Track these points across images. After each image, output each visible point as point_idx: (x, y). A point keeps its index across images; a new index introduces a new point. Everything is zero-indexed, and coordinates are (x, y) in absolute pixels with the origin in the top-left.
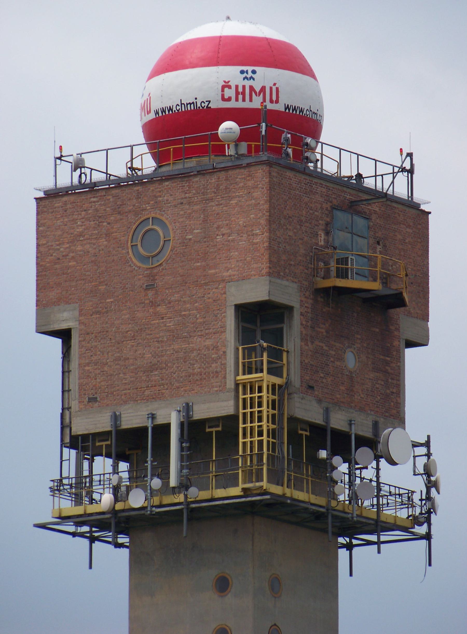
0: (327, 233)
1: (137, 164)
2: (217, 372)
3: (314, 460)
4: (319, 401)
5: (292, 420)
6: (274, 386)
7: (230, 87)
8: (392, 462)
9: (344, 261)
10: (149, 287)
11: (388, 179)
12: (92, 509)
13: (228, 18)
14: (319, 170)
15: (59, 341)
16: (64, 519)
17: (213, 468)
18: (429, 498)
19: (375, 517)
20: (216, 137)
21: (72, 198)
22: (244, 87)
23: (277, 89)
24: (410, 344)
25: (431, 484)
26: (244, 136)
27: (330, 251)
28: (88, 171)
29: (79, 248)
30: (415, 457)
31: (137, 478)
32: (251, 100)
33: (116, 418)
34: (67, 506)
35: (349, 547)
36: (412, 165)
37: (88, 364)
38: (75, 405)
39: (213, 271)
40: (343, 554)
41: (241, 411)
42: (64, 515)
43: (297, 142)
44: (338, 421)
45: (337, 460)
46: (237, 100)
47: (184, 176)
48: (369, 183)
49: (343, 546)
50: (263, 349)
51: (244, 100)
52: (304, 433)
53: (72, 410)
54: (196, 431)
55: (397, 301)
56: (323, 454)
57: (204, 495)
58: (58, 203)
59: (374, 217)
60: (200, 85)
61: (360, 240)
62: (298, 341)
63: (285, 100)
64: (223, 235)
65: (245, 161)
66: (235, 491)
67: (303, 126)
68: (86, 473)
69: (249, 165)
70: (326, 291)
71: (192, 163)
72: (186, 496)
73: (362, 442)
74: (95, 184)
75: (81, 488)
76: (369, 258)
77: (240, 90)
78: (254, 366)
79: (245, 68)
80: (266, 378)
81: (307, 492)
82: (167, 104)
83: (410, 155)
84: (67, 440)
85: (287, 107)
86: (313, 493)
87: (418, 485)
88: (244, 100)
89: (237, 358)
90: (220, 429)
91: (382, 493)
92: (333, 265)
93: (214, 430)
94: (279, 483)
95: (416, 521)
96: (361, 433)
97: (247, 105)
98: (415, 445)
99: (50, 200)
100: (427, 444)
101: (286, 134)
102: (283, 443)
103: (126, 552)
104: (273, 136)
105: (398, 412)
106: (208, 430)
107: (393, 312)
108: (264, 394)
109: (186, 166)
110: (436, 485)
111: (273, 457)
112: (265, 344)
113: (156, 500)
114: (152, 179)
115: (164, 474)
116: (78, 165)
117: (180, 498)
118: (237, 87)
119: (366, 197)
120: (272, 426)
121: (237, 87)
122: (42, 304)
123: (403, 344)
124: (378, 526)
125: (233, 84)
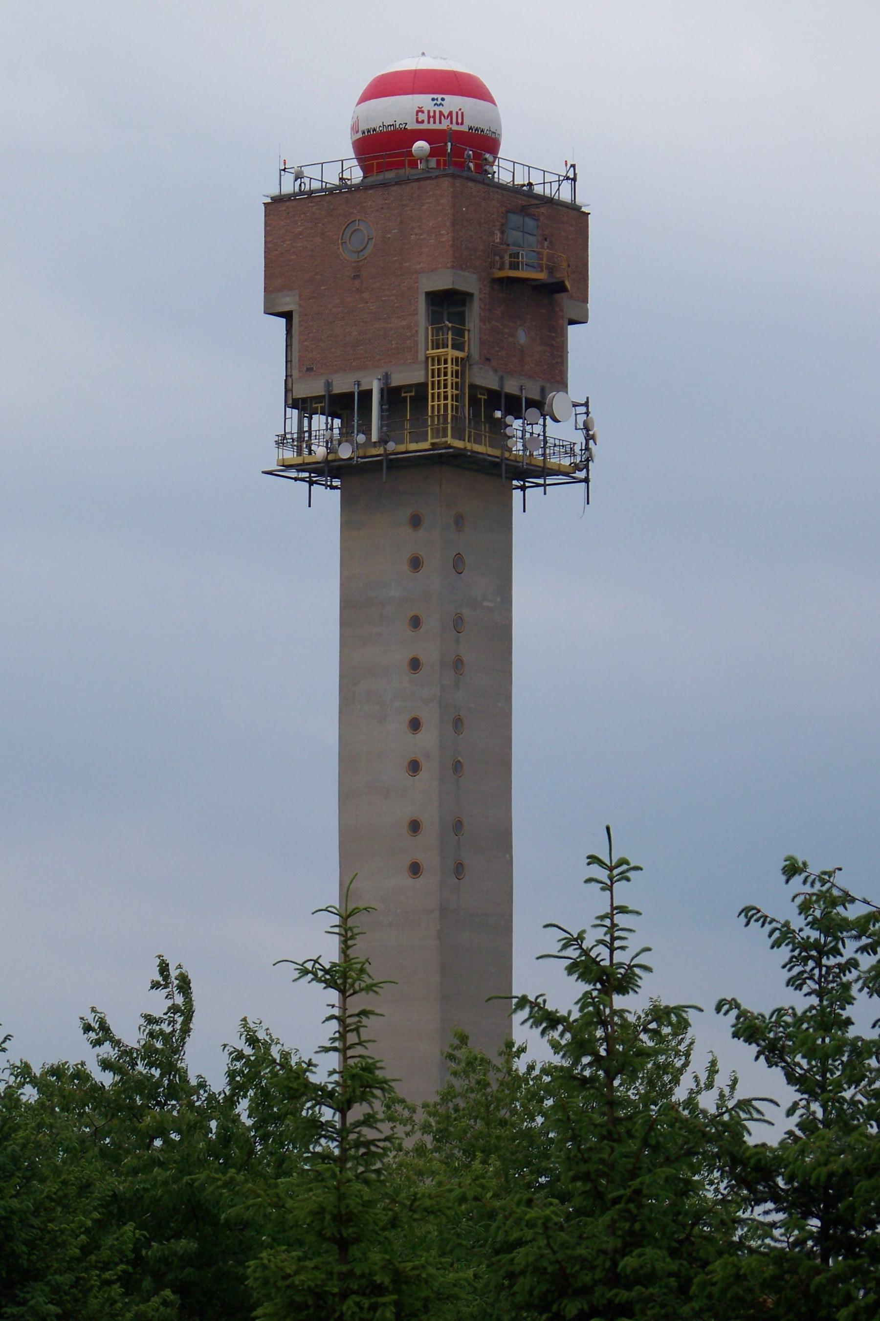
0: (502, 232)
1: (346, 175)
2: (411, 348)
3: (490, 418)
4: (495, 371)
5: (472, 387)
6: (457, 359)
7: (423, 112)
8: (556, 421)
9: (515, 255)
10: (356, 277)
11: (555, 186)
12: (309, 459)
13: (423, 54)
14: (496, 180)
15: (284, 320)
16: (288, 467)
17: (407, 425)
18: (587, 449)
19: (542, 465)
20: (410, 154)
21: (294, 203)
22: (435, 111)
23: (462, 113)
24: (572, 322)
25: (589, 437)
26: (433, 153)
27: (504, 247)
28: (307, 181)
29: (299, 245)
30: (576, 415)
31: (346, 434)
32: (440, 123)
33: (328, 385)
34: (289, 455)
35: (523, 488)
36: (575, 174)
37: (306, 340)
38: (295, 374)
39: (407, 264)
40: (517, 494)
41: (430, 379)
42: (286, 464)
43: (477, 156)
44: (511, 387)
45: (509, 419)
46: (429, 122)
47: (385, 185)
48: (538, 190)
49: (518, 488)
50: (449, 329)
51: (435, 122)
52: (483, 397)
53: (294, 377)
54: (393, 396)
55: (561, 288)
56: (498, 414)
57: (402, 448)
58: (282, 207)
59: (542, 218)
60: (401, 110)
61: (530, 238)
62: (477, 321)
63: (469, 122)
64: (416, 234)
65: (433, 175)
66: (425, 445)
67: (485, 144)
68: (306, 429)
69: (437, 177)
70: (500, 280)
71: (391, 175)
72: (385, 449)
73: (531, 404)
74: (312, 192)
75: (302, 441)
76: (538, 253)
77: (432, 114)
78: (441, 342)
79: (435, 96)
80: (451, 353)
81: (485, 445)
82: (372, 125)
83: (573, 166)
84: (290, 402)
85: (470, 128)
86: (490, 446)
87: (579, 438)
88: (435, 122)
89: (427, 337)
90: (413, 394)
91: (548, 445)
92: (507, 259)
93: (408, 395)
94: (461, 438)
95: (577, 467)
96: (530, 396)
97: (437, 126)
98: (575, 405)
99: (277, 206)
100: (586, 405)
101: (473, 149)
102: (465, 405)
103: (338, 492)
104: (458, 152)
105: (562, 378)
106: (403, 395)
107: (557, 296)
108: (449, 365)
109: (386, 177)
110: (593, 438)
111: (456, 417)
112: (450, 325)
113: (361, 453)
114: (357, 187)
115: (367, 432)
116: (299, 176)
117: (381, 451)
118: (429, 112)
119: (538, 202)
120: (455, 392)
121: (429, 112)
122: (268, 290)
123: (566, 322)
124: (544, 471)
125: (425, 109)
